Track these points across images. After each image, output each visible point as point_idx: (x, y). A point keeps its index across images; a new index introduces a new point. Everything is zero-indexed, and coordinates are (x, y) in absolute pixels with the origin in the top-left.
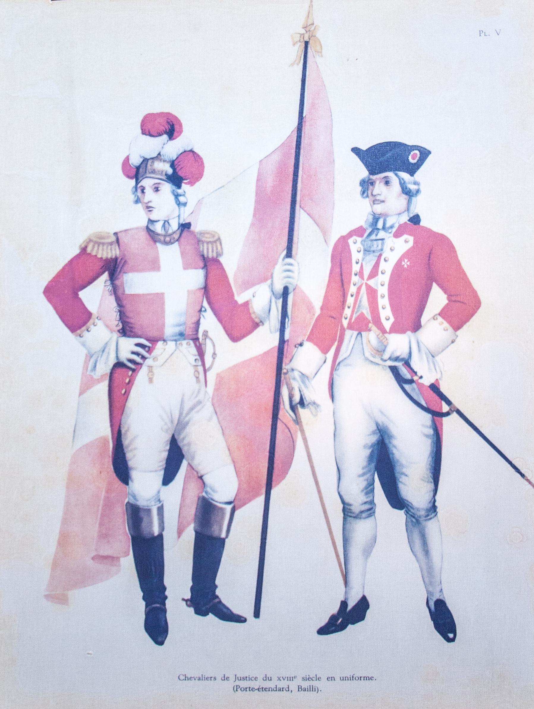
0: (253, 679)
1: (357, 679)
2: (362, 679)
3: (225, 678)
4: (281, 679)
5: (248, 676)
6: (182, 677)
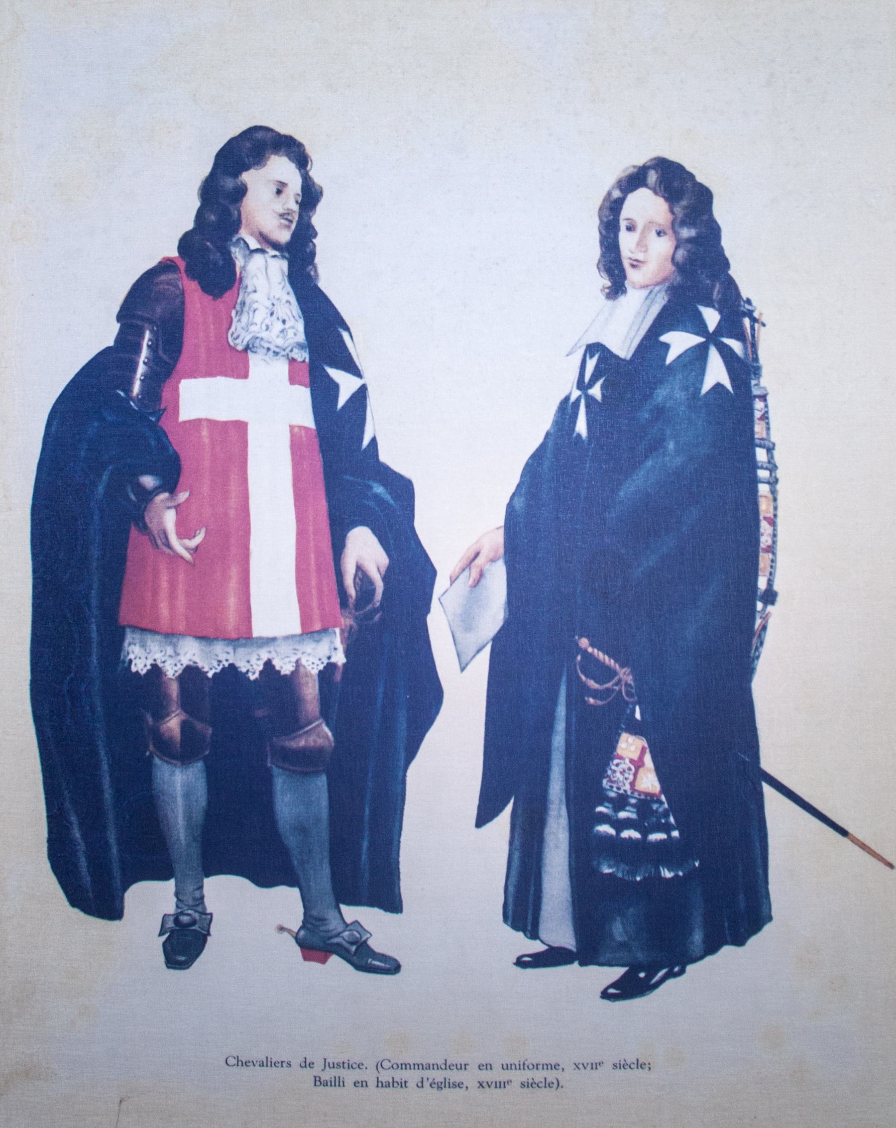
0: (354, 1066)
1: (531, 1067)
2: (540, 1067)
3: (307, 1064)
4: (581, 1066)
5: (346, 1061)
6: (232, 1061)
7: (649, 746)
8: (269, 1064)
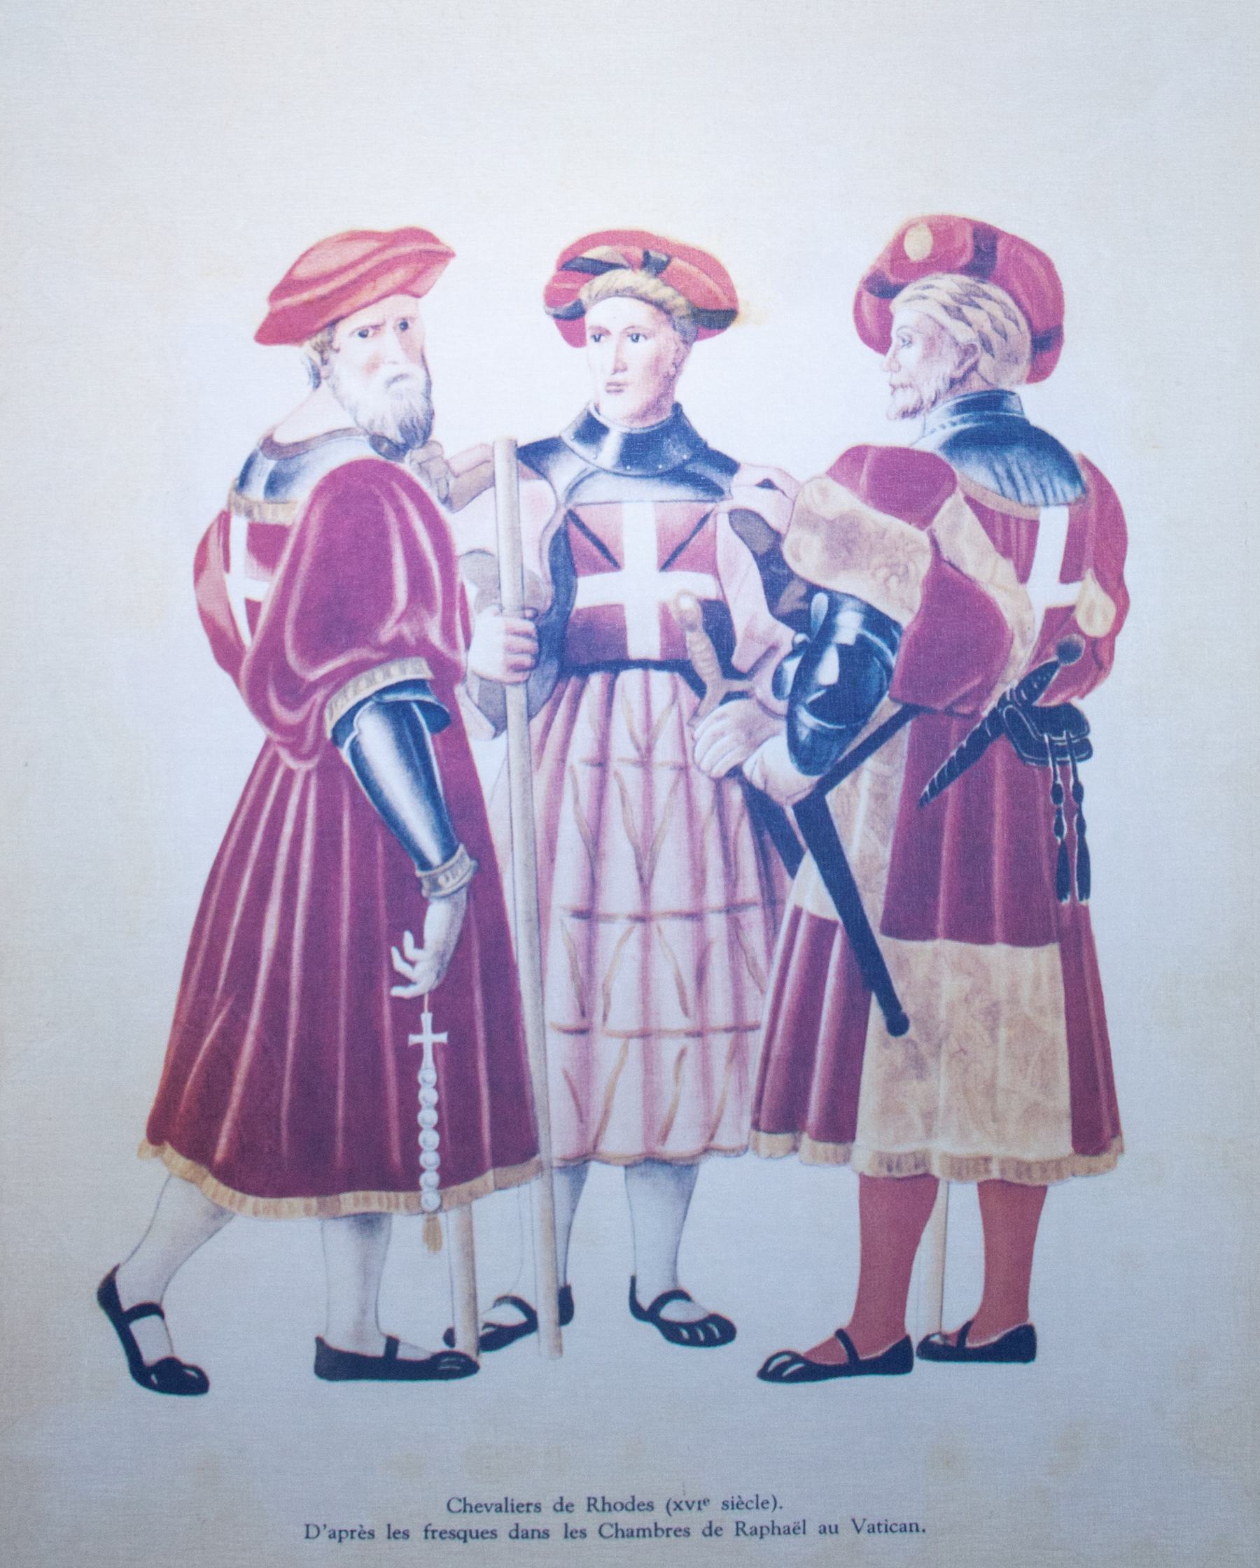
0: (894, 1528)
4: (683, 1506)
6: (456, 1506)
7: (846, 922)
8: (509, 1508)
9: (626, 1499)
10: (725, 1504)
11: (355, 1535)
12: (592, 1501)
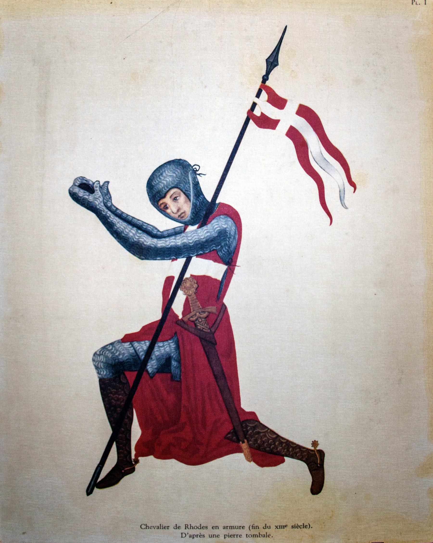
2: (228, 528)
6: (143, 527)
9: (198, 525)
10: (292, 527)
11: (198, 536)
12: (187, 526)
